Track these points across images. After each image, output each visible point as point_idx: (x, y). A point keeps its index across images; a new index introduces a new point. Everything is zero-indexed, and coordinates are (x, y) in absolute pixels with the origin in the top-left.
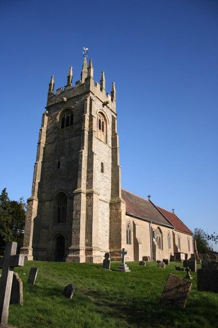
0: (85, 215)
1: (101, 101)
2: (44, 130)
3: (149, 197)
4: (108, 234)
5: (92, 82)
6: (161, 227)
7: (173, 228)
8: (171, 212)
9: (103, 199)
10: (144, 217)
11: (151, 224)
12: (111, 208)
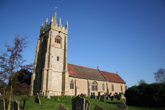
0: (46, 78)
1: (58, 31)
2: (38, 46)
3: (98, 67)
4: (61, 85)
5: (52, 24)
6: (97, 81)
7: (107, 81)
8: (116, 73)
9: (58, 71)
10: (84, 77)
11: (88, 80)
12: (63, 75)
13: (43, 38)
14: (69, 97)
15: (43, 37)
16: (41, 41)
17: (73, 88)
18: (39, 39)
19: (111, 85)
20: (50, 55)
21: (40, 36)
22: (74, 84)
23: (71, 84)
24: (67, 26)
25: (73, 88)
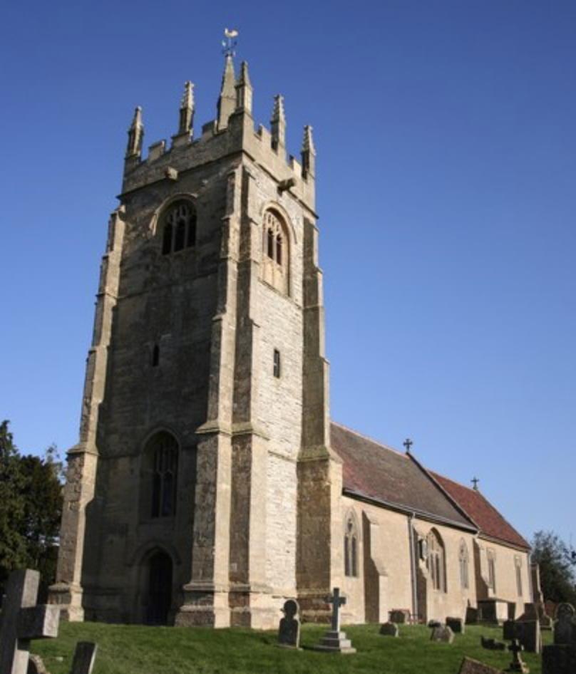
1: (274, 179)
2: (115, 257)
4: (293, 549)
8: (470, 486)
11: (414, 521)
13: (158, 211)
14: (34, 569)
15: (160, 202)
16: (137, 227)
17: (355, 574)
18: (123, 217)
19: (512, 557)
20: (254, 334)
21: (125, 198)
22: (360, 545)
23: (346, 540)
24: (312, 160)
25: (355, 574)
